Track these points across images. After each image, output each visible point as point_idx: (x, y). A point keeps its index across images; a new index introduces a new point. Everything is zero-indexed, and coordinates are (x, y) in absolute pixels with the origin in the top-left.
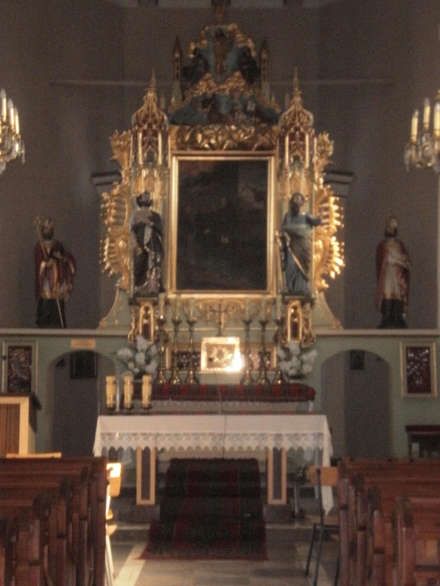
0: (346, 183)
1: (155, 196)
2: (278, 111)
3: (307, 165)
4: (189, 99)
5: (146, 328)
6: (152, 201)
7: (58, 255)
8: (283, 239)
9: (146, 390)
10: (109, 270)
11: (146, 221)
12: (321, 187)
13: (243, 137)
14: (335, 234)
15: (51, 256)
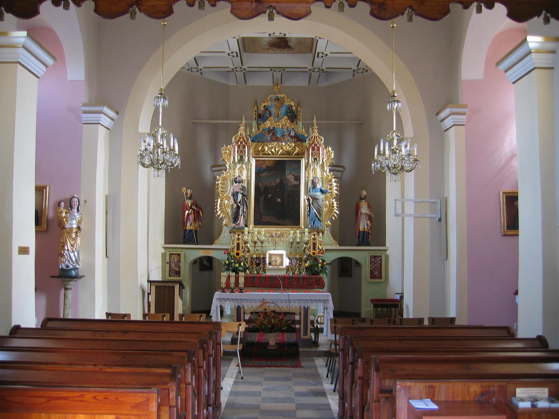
0: (340, 171)
1: (244, 177)
2: (306, 135)
3: (321, 163)
4: (261, 129)
5: (238, 244)
6: (242, 180)
7: (194, 207)
8: (308, 200)
9: (242, 280)
10: (220, 215)
11: (239, 190)
12: (328, 174)
13: (288, 149)
14: (334, 198)
15: (191, 207)
